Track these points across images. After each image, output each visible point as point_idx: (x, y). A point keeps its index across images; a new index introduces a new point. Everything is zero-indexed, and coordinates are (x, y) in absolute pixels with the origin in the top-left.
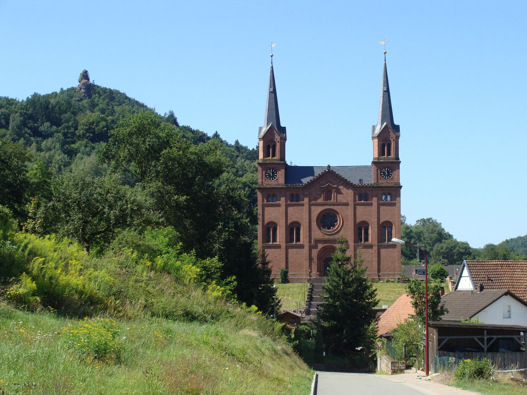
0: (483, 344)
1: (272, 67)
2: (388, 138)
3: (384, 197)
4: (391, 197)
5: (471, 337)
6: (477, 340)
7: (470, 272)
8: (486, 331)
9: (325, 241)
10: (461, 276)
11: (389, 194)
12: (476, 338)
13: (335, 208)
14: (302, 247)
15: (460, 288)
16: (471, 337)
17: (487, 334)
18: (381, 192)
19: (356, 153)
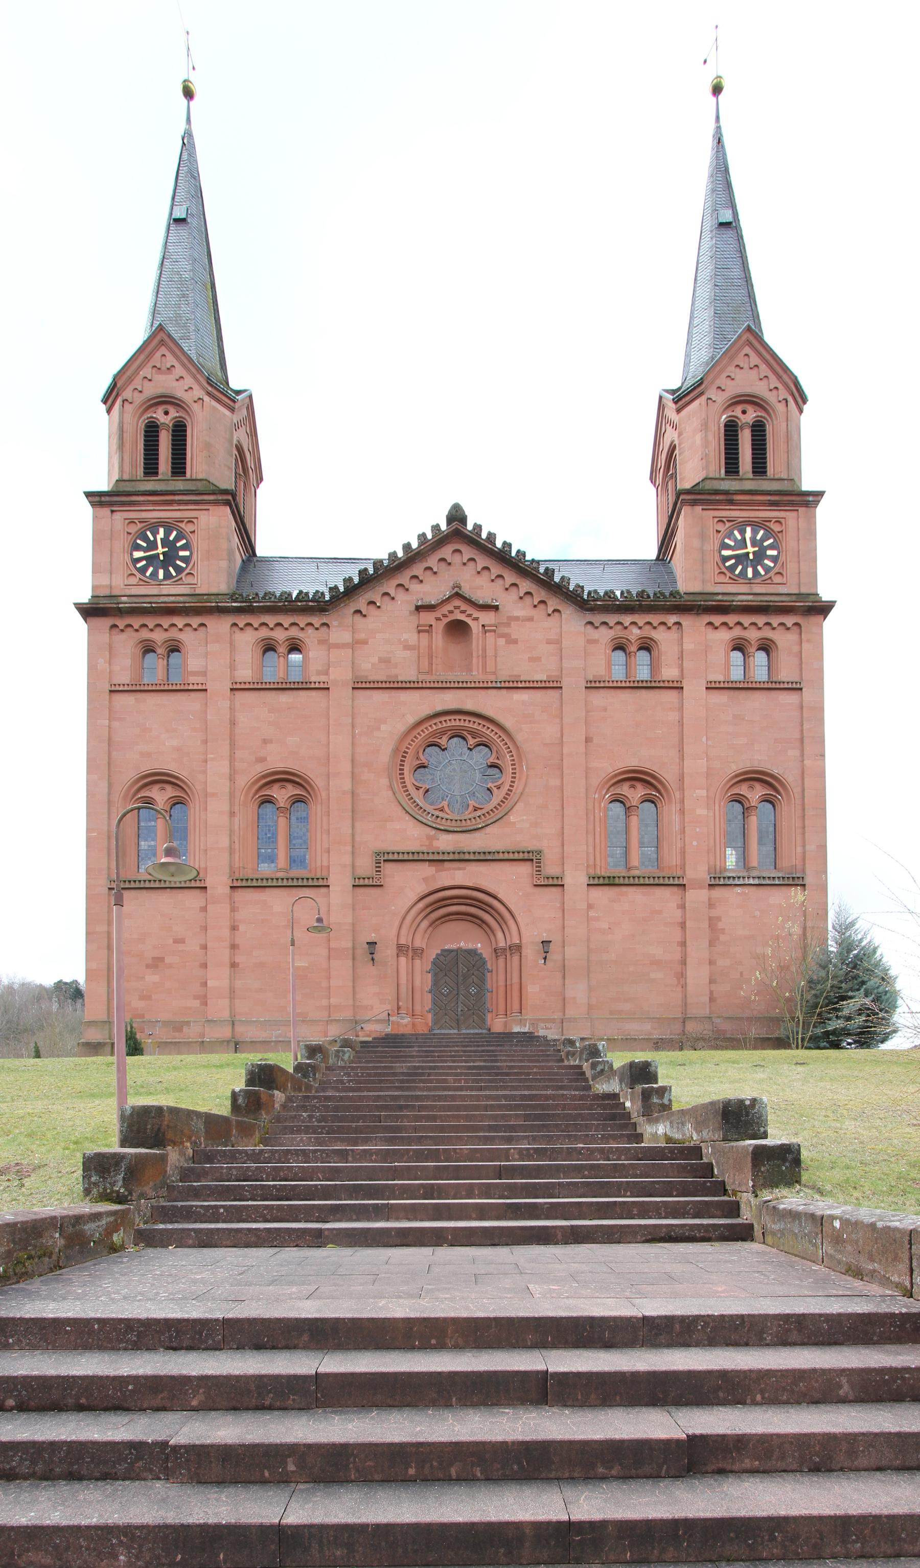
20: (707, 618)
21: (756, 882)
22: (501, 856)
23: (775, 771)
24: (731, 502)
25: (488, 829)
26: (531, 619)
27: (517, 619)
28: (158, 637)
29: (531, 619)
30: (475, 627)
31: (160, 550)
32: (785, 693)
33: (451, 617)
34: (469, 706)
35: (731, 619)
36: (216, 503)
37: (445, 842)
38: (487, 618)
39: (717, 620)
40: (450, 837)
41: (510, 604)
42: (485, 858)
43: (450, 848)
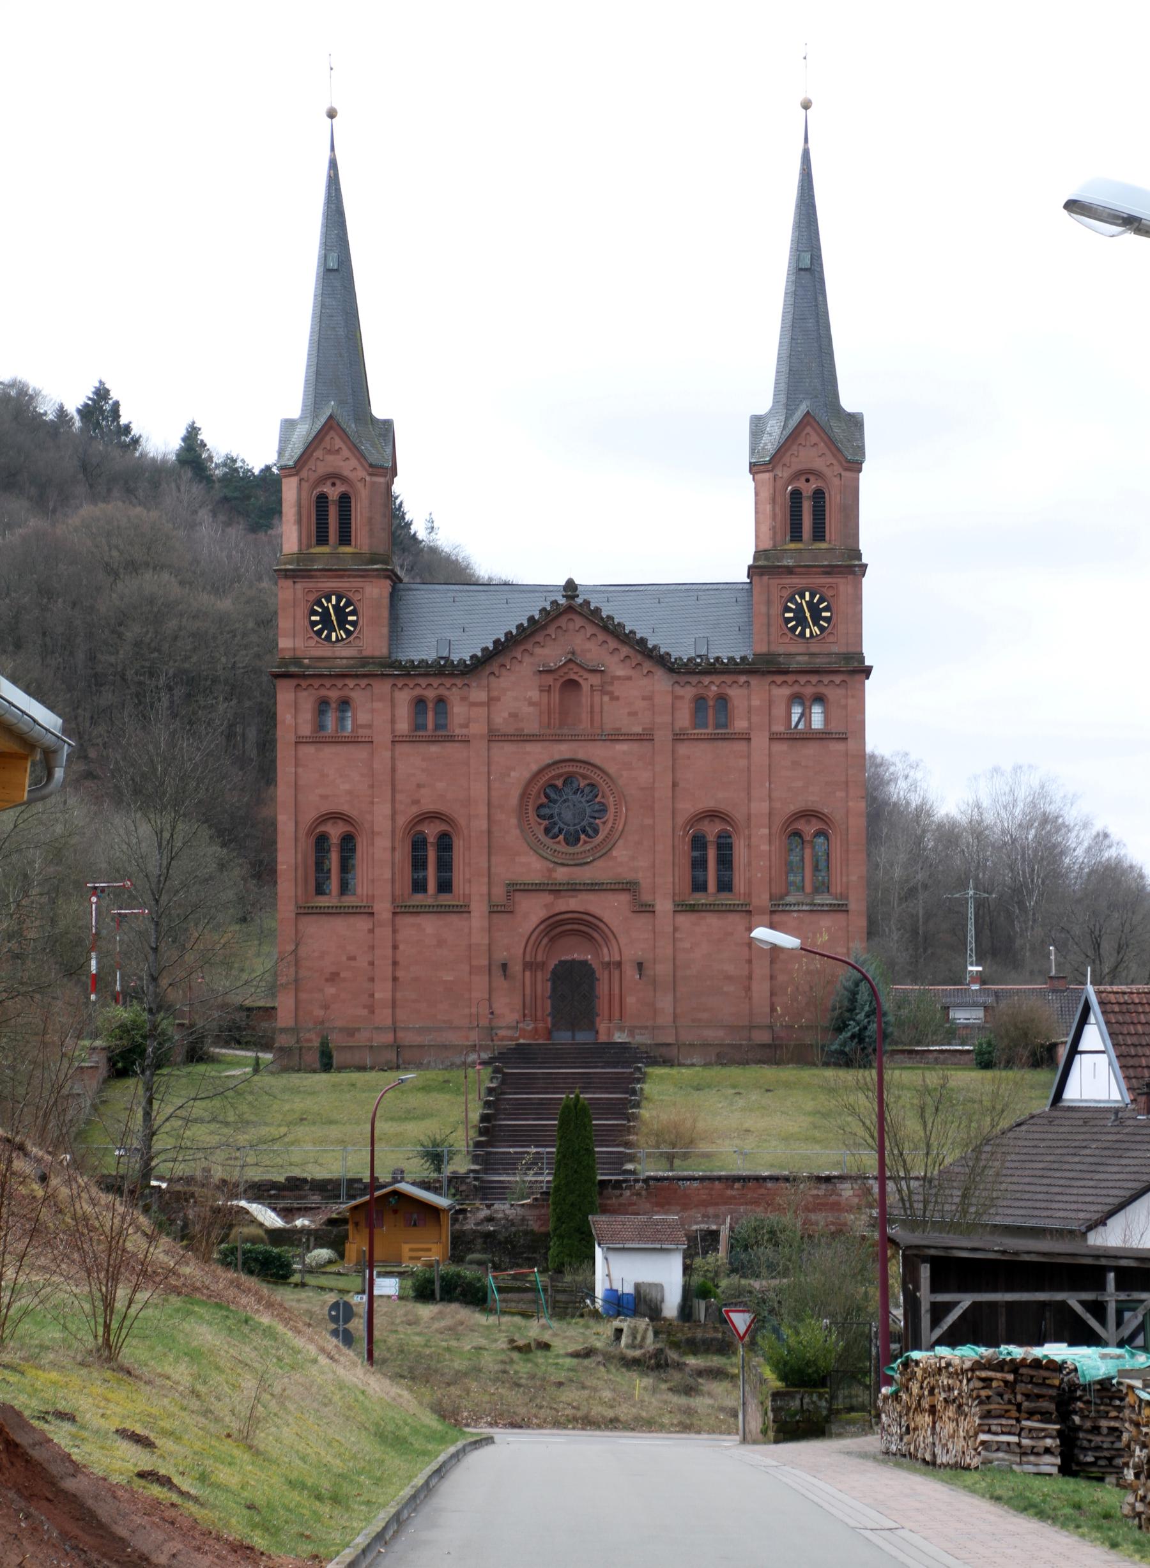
0: (1103, 1321)
1: (333, 165)
2: (810, 477)
3: (797, 711)
4: (826, 714)
5: (1059, 1296)
6: (1079, 1309)
7: (1115, 1034)
8: (1111, 1276)
9: (556, 890)
10: (1074, 1051)
11: (819, 699)
12: (1073, 1300)
13: (596, 753)
14: (463, 910)
15: (1072, 1093)
16: (1059, 1296)
17: (1119, 1288)
18: (786, 691)
19: (689, 532)
20: (770, 678)
25: (595, 863)
26: (629, 678)
27: (619, 678)
29: (629, 678)
30: (586, 687)
34: (581, 755)
37: (562, 874)
38: (595, 680)
42: (594, 888)
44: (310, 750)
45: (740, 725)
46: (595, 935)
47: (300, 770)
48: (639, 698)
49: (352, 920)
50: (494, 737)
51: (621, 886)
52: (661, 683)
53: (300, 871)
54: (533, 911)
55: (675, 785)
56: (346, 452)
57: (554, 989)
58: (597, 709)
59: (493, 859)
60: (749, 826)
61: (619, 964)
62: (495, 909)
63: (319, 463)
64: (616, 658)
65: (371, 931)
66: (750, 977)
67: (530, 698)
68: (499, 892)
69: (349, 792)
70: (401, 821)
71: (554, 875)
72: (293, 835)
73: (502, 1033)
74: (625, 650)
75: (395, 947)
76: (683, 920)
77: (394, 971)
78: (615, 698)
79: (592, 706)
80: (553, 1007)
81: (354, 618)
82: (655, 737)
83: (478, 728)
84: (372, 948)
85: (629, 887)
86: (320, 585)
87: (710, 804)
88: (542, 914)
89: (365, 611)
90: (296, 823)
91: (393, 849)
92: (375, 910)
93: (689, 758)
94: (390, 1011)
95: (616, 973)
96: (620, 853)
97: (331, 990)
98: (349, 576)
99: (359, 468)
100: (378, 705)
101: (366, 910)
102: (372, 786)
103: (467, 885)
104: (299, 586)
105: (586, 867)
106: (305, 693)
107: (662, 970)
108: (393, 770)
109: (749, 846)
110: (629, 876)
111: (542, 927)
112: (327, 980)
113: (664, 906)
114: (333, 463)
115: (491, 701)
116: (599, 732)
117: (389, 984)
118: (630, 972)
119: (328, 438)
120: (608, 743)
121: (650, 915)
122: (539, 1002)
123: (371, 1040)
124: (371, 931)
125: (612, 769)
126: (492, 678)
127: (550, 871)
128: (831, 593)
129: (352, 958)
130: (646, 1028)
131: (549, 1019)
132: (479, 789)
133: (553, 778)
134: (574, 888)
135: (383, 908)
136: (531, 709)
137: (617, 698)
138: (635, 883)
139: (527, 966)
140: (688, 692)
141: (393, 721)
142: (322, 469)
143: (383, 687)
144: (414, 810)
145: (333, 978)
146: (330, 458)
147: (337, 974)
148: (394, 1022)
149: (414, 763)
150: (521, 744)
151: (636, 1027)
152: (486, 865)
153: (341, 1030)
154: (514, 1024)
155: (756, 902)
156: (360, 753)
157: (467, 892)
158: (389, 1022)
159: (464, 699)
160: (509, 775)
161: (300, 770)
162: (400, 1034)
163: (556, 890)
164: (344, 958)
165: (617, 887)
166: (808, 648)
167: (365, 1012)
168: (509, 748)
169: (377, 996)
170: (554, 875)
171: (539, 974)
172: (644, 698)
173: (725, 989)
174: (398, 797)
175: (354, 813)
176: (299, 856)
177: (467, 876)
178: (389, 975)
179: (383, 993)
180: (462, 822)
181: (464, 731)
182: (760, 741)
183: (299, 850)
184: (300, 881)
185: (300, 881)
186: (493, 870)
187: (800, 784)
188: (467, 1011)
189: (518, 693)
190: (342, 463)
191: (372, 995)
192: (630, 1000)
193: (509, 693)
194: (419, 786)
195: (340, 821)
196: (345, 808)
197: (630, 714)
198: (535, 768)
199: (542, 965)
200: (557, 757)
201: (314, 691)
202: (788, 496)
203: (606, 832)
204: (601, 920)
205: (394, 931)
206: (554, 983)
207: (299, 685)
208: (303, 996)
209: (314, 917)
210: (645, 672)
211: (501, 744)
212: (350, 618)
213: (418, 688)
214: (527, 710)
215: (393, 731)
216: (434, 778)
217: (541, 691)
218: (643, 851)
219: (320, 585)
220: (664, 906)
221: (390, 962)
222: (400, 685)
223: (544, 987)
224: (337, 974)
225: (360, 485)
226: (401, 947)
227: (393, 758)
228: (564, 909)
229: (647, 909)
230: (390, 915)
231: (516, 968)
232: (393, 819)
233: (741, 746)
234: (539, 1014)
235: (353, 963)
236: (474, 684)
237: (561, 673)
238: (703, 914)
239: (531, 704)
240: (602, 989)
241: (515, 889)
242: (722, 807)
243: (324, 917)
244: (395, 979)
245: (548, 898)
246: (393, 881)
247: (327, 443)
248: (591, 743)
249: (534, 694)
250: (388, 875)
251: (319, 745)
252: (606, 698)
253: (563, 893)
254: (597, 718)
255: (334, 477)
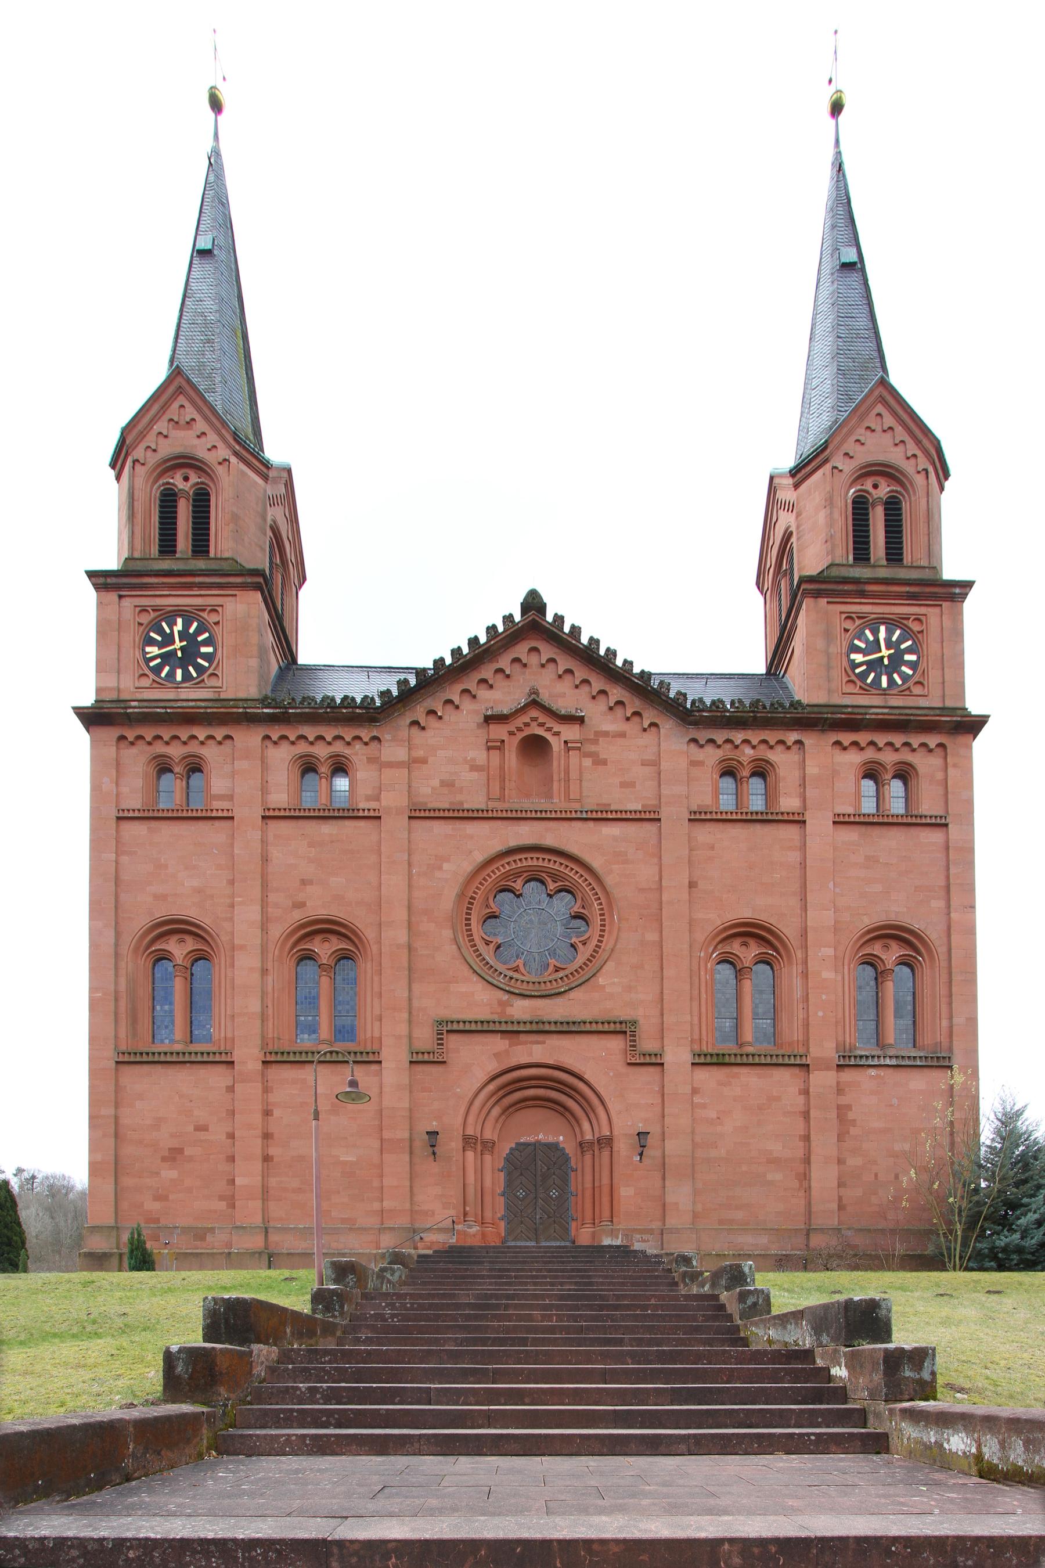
2: (866, 526)
9: (512, 1031)
18: (855, 758)
20: (834, 737)
21: (894, 1062)
22: (588, 1028)
23: (916, 926)
24: (862, 594)
25: (572, 994)
26: (622, 735)
27: (606, 734)
28: (176, 751)
29: (622, 735)
30: (556, 744)
31: (178, 644)
32: (927, 830)
33: (527, 732)
34: (549, 841)
35: (863, 738)
36: (243, 587)
37: (521, 1009)
38: (570, 732)
39: (846, 738)
40: (526, 1003)
41: (595, 713)
42: (569, 1029)
43: (526, 1017)
44: (138, 830)
45: (789, 803)
46: (570, 1103)
47: (125, 859)
48: (625, 761)
49: (202, 1071)
50: (419, 814)
51: (612, 1027)
52: (672, 741)
53: (123, 1004)
54: (478, 1061)
55: (692, 885)
56: (201, 425)
57: (509, 1183)
58: (574, 775)
59: (416, 987)
60: (805, 947)
61: (607, 1142)
62: (420, 1058)
63: (161, 439)
64: (601, 705)
65: (231, 1089)
66: (807, 1160)
67: (473, 760)
68: (424, 1037)
69: (199, 891)
70: (277, 931)
71: (509, 1011)
72: (112, 951)
73: (429, 1237)
74: (617, 693)
75: (267, 1113)
76: (707, 1077)
77: (265, 1147)
78: (600, 762)
79: (567, 772)
80: (508, 1207)
81: (210, 650)
82: (663, 816)
83: (394, 799)
84: (232, 1113)
85: (622, 1029)
86: (159, 601)
87: (746, 913)
88: (493, 1067)
89: (226, 637)
90: (118, 935)
91: (264, 972)
92: (235, 1059)
93: (712, 848)
94: (259, 1203)
95: (606, 1153)
96: (609, 979)
97: (169, 1174)
98: (201, 586)
99: (220, 445)
100: (241, 765)
101: (224, 1058)
102: (232, 882)
103: (377, 1024)
104: (127, 603)
105: (559, 1000)
106: (134, 750)
107: (676, 1147)
108: (265, 859)
109: (805, 975)
110: (624, 1014)
111: (491, 1087)
112: (164, 1159)
113: (677, 1056)
114: (183, 441)
115: (413, 763)
116: (577, 806)
117: (258, 1165)
118: (623, 1147)
119: (175, 405)
120: (591, 824)
121: (658, 1069)
122: (488, 1199)
123: (229, 1245)
124: (231, 1089)
125: (596, 862)
126: (415, 730)
127: (502, 1004)
128: (915, 627)
129: (201, 1128)
130: (650, 1231)
131: (502, 1224)
132: (394, 884)
133: (507, 876)
134: (540, 1029)
135: (248, 1056)
136: (475, 775)
137: (604, 762)
138: (634, 1023)
139: (468, 1142)
140: (711, 756)
141: (264, 790)
142: (166, 449)
143: (249, 738)
144: (297, 916)
145: (174, 1155)
146: (176, 434)
147: (180, 1151)
148: (266, 1219)
149: (294, 848)
150: (458, 824)
151: (635, 1230)
152: (406, 995)
153: (185, 1230)
154: (448, 1223)
155: (815, 1052)
156: (213, 834)
157: (376, 1034)
158: (258, 1220)
159: (371, 760)
160: (440, 868)
161: (125, 859)
162: (274, 1238)
163: (512, 1031)
164: (191, 1128)
165: (606, 1028)
166: (886, 702)
167: (223, 1205)
168: (439, 828)
169: (238, 1181)
170: (509, 1011)
171: (488, 1158)
172: (644, 763)
173: (770, 1177)
174: (272, 898)
175: (206, 920)
176: (123, 981)
177: (377, 1012)
178: (258, 1152)
179: (248, 1176)
180: (369, 934)
181: (373, 805)
182: (819, 823)
183: (122, 972)
184: (123, 1016)
185: (123, 1016)
186: (416, 1003)
187: (878, 888)
188: (376, 1206)
189: (453, 752)
190: (196, 441)
191: (232, 1182)
192: (625, 1192)
193: (441, 753)
194: (304, 882)
195: (187, 937)
196: (190, 911)
197: (624, 785)
198: (480, 857)
199: (488, 1146)
200: (513, 843)
201: (148, 748)
202: (850, 501)
203: (587, 955)
204: (581, 1078)
205: (266, 1090)
206: (509, 1174)
207: (122, 738)
208: (127, 1181)
209: (146, 1068)
210: (646, 725)
211: (428, 823)
212: (204, 650)
213: (159, 742)
214: (468, 777)
215: (264, 801)
216: (318, 872)
217: (489, 749)
218: (649, 978)
219: (159, 601)
220: (677, 1056)
221: (259, 1132)
222: (275, 738)
223: (494, 1180)
224: (180, 1151)
225: (221, 470)
226: (277, 1113)
227: (264, 842)
228: (524, 1060)
229: (654, 1062)
230: (259, 1066)
231: (451, 1145)
232: (264, 928)
233: (791, 832)
234: (488, 1214)
235: (202, 1135)
236: (388, 737)
237: (520, 721)
238: (736, 1070)
239: (474, 768)
240: (581, 1181)
241: (450, 1029)
242: (763, 917)
243: (159, 1068)
244: (267, 1159)
245: (499, 1043)
246: (264, 1018)
247: (173, 411)
248: (566, 824)
249: (480, 755)
250: (255, 1006)
251: (154, 824)
252: (587, 762)
253: (523, 1037)
254: (574, 787)
255: (185, 462)
